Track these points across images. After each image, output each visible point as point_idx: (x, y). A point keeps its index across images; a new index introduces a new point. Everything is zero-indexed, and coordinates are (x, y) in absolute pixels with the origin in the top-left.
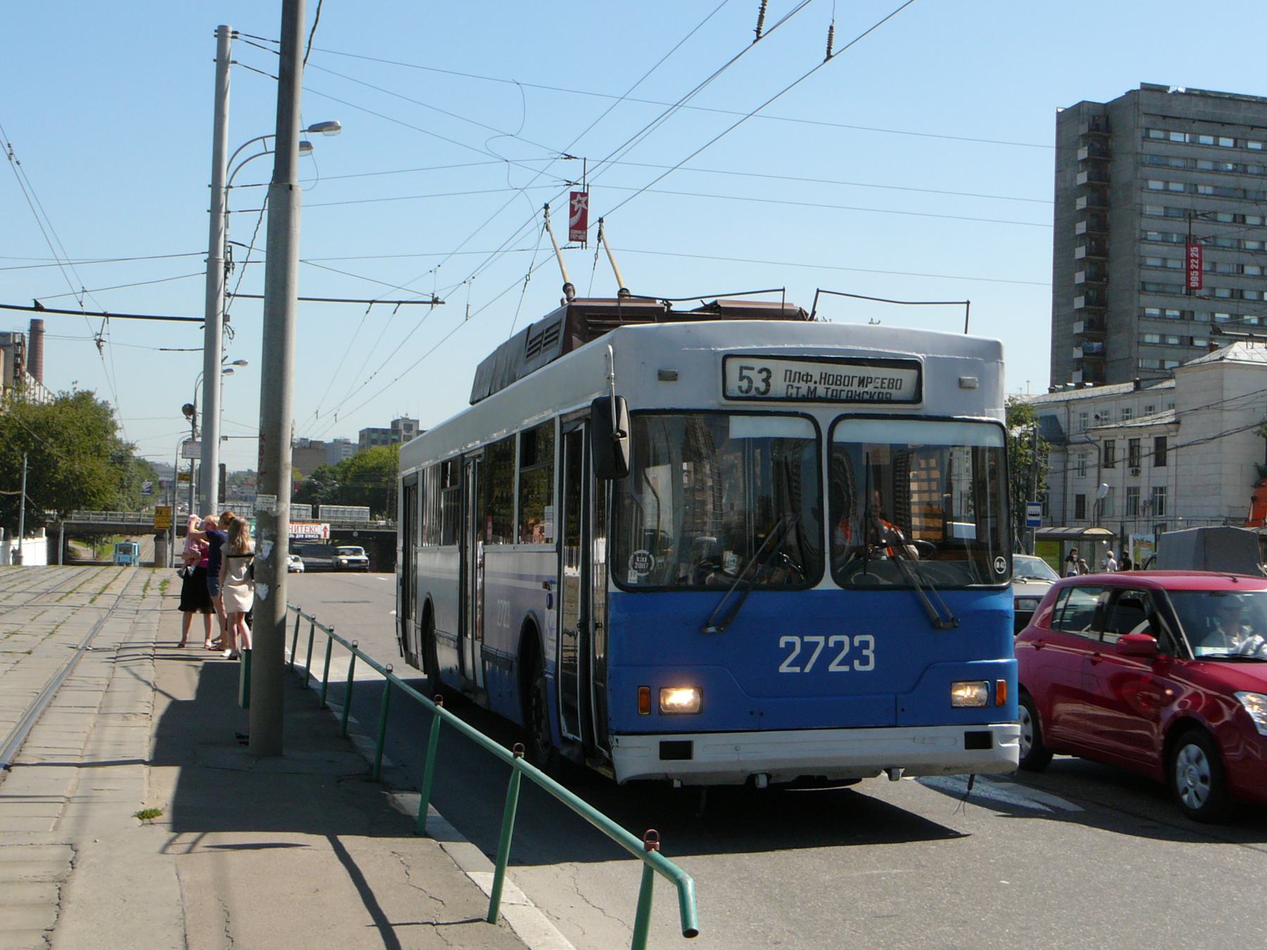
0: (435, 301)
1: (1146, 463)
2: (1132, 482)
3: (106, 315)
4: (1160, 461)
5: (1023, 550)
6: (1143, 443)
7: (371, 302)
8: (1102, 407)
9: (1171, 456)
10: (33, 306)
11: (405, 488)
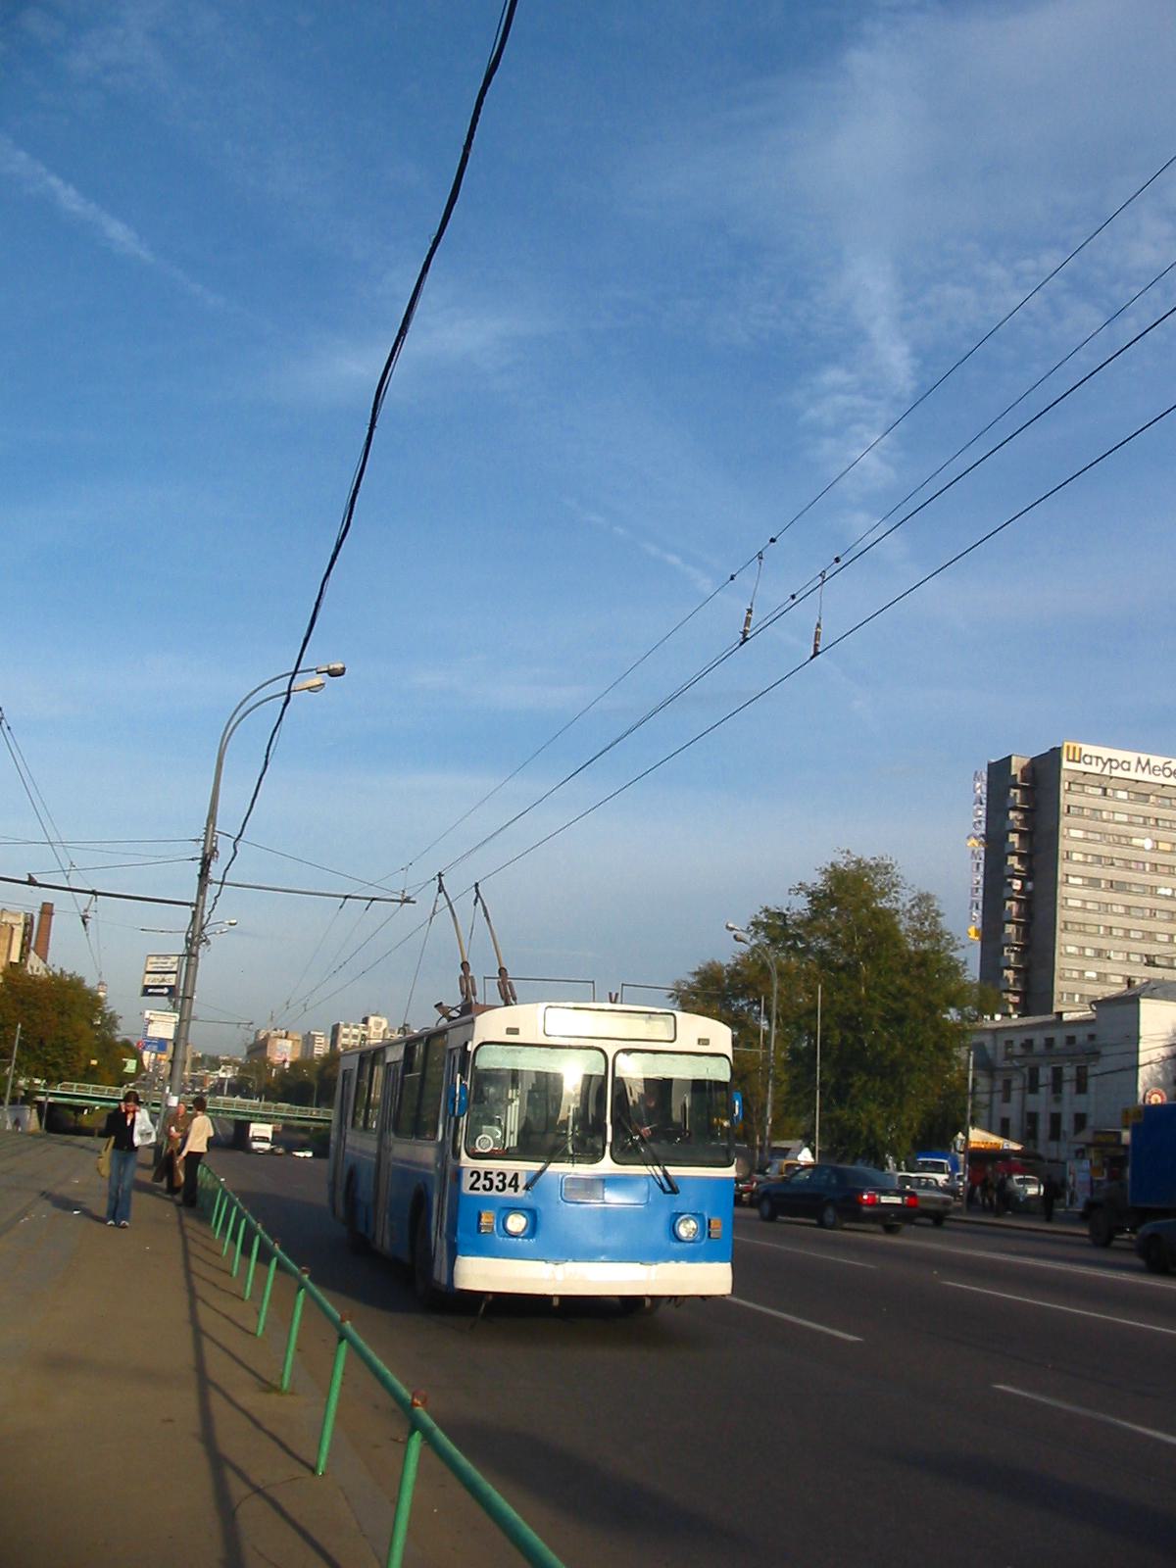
0: (407, 900)
1: (1068, 1088)
2: (1055, 1109)
3: (93, 892)
4: (1081, 1088)
5: (635, 1093)
6: (1065, 1070)
7: (346, 897)
8: (1028, 1035)
9: (1092, 1081)
10: (27, 880)
11: (344, 1075)
